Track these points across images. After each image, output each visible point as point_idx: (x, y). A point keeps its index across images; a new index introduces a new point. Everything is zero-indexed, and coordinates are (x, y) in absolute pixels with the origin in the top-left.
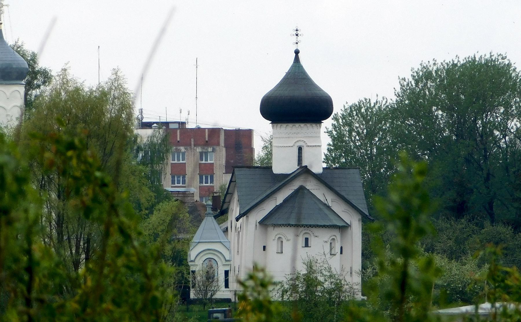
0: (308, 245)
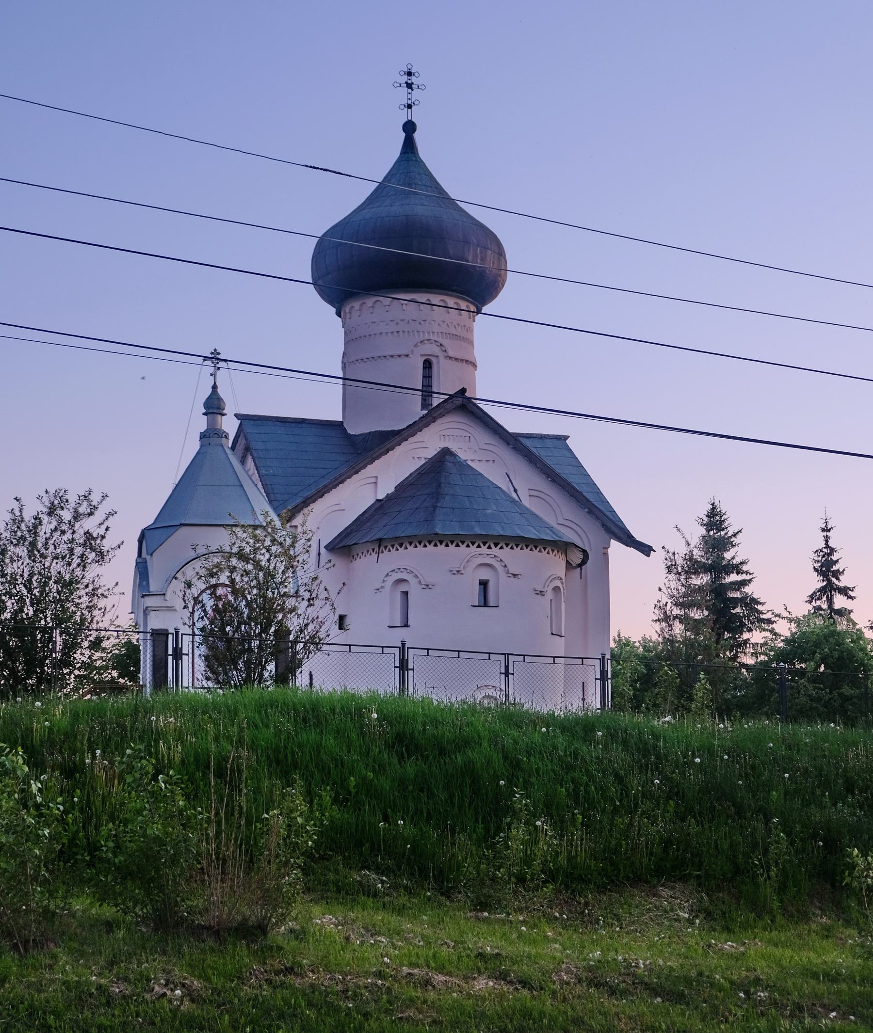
0: (492, 601)
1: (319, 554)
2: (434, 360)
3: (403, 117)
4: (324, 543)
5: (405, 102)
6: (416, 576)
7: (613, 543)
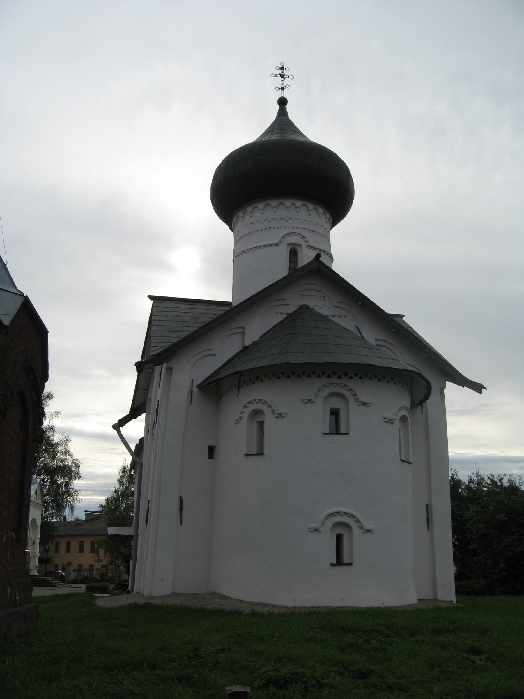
0: (343, 430)
1: (192, 392)
2: (299, 249)
3: (278, 95)
4: (197, 382)
5: (280, 86)
6: (270, 406)
7: (448, 384)
